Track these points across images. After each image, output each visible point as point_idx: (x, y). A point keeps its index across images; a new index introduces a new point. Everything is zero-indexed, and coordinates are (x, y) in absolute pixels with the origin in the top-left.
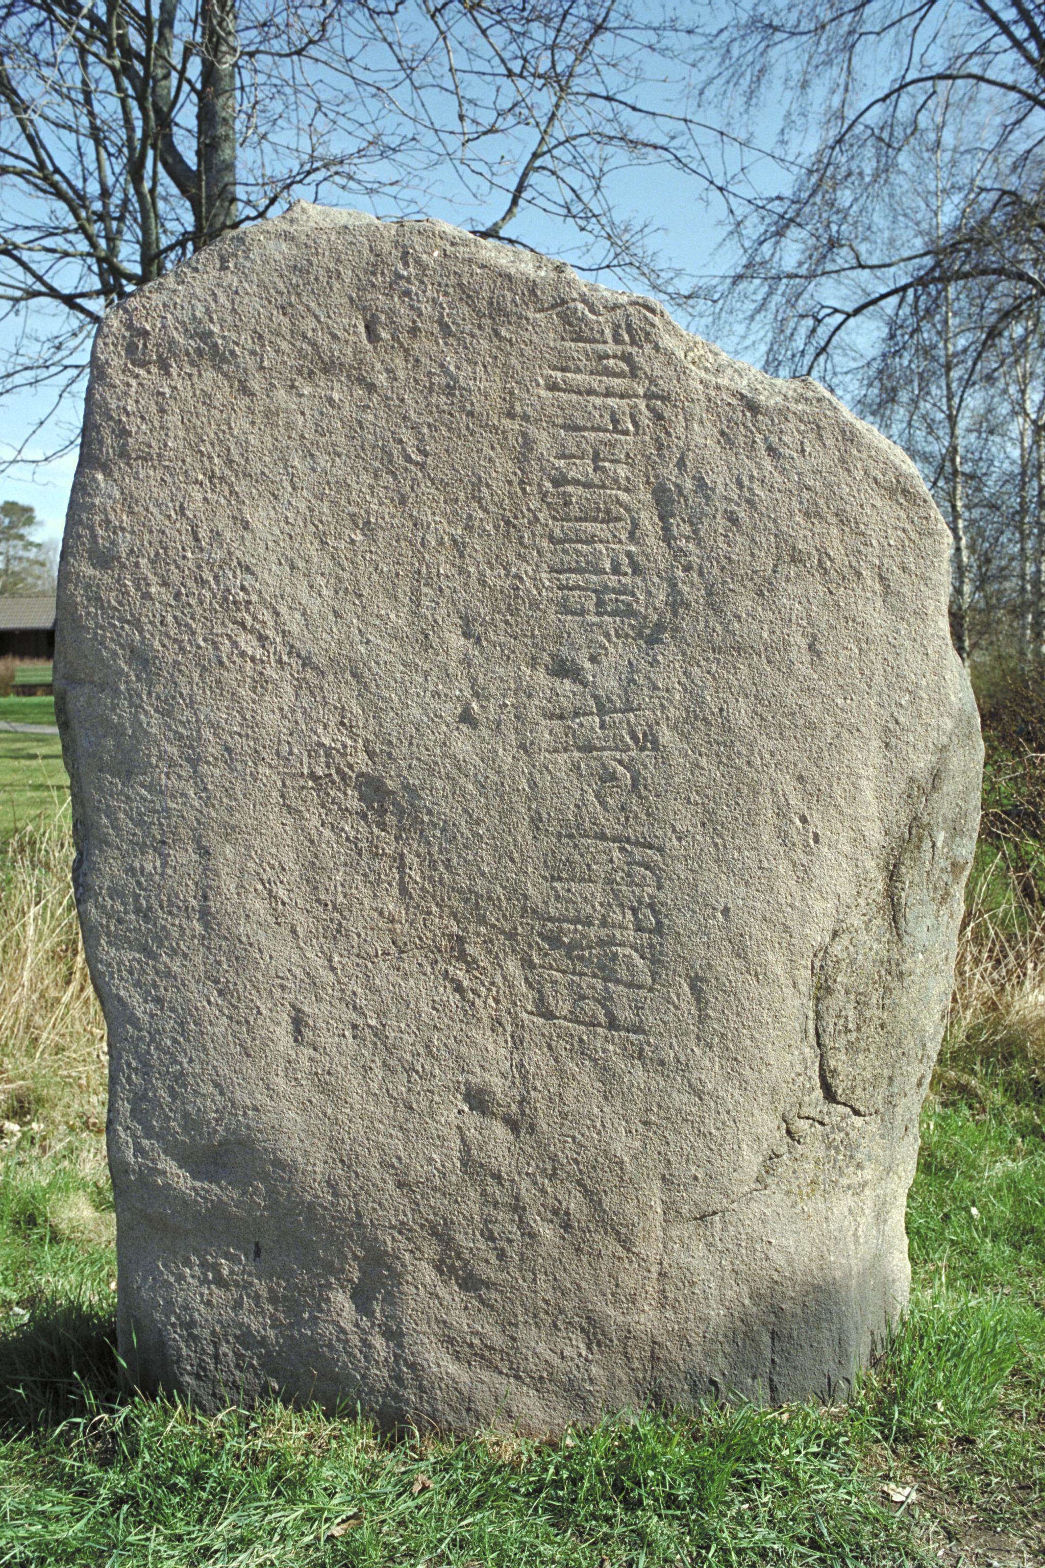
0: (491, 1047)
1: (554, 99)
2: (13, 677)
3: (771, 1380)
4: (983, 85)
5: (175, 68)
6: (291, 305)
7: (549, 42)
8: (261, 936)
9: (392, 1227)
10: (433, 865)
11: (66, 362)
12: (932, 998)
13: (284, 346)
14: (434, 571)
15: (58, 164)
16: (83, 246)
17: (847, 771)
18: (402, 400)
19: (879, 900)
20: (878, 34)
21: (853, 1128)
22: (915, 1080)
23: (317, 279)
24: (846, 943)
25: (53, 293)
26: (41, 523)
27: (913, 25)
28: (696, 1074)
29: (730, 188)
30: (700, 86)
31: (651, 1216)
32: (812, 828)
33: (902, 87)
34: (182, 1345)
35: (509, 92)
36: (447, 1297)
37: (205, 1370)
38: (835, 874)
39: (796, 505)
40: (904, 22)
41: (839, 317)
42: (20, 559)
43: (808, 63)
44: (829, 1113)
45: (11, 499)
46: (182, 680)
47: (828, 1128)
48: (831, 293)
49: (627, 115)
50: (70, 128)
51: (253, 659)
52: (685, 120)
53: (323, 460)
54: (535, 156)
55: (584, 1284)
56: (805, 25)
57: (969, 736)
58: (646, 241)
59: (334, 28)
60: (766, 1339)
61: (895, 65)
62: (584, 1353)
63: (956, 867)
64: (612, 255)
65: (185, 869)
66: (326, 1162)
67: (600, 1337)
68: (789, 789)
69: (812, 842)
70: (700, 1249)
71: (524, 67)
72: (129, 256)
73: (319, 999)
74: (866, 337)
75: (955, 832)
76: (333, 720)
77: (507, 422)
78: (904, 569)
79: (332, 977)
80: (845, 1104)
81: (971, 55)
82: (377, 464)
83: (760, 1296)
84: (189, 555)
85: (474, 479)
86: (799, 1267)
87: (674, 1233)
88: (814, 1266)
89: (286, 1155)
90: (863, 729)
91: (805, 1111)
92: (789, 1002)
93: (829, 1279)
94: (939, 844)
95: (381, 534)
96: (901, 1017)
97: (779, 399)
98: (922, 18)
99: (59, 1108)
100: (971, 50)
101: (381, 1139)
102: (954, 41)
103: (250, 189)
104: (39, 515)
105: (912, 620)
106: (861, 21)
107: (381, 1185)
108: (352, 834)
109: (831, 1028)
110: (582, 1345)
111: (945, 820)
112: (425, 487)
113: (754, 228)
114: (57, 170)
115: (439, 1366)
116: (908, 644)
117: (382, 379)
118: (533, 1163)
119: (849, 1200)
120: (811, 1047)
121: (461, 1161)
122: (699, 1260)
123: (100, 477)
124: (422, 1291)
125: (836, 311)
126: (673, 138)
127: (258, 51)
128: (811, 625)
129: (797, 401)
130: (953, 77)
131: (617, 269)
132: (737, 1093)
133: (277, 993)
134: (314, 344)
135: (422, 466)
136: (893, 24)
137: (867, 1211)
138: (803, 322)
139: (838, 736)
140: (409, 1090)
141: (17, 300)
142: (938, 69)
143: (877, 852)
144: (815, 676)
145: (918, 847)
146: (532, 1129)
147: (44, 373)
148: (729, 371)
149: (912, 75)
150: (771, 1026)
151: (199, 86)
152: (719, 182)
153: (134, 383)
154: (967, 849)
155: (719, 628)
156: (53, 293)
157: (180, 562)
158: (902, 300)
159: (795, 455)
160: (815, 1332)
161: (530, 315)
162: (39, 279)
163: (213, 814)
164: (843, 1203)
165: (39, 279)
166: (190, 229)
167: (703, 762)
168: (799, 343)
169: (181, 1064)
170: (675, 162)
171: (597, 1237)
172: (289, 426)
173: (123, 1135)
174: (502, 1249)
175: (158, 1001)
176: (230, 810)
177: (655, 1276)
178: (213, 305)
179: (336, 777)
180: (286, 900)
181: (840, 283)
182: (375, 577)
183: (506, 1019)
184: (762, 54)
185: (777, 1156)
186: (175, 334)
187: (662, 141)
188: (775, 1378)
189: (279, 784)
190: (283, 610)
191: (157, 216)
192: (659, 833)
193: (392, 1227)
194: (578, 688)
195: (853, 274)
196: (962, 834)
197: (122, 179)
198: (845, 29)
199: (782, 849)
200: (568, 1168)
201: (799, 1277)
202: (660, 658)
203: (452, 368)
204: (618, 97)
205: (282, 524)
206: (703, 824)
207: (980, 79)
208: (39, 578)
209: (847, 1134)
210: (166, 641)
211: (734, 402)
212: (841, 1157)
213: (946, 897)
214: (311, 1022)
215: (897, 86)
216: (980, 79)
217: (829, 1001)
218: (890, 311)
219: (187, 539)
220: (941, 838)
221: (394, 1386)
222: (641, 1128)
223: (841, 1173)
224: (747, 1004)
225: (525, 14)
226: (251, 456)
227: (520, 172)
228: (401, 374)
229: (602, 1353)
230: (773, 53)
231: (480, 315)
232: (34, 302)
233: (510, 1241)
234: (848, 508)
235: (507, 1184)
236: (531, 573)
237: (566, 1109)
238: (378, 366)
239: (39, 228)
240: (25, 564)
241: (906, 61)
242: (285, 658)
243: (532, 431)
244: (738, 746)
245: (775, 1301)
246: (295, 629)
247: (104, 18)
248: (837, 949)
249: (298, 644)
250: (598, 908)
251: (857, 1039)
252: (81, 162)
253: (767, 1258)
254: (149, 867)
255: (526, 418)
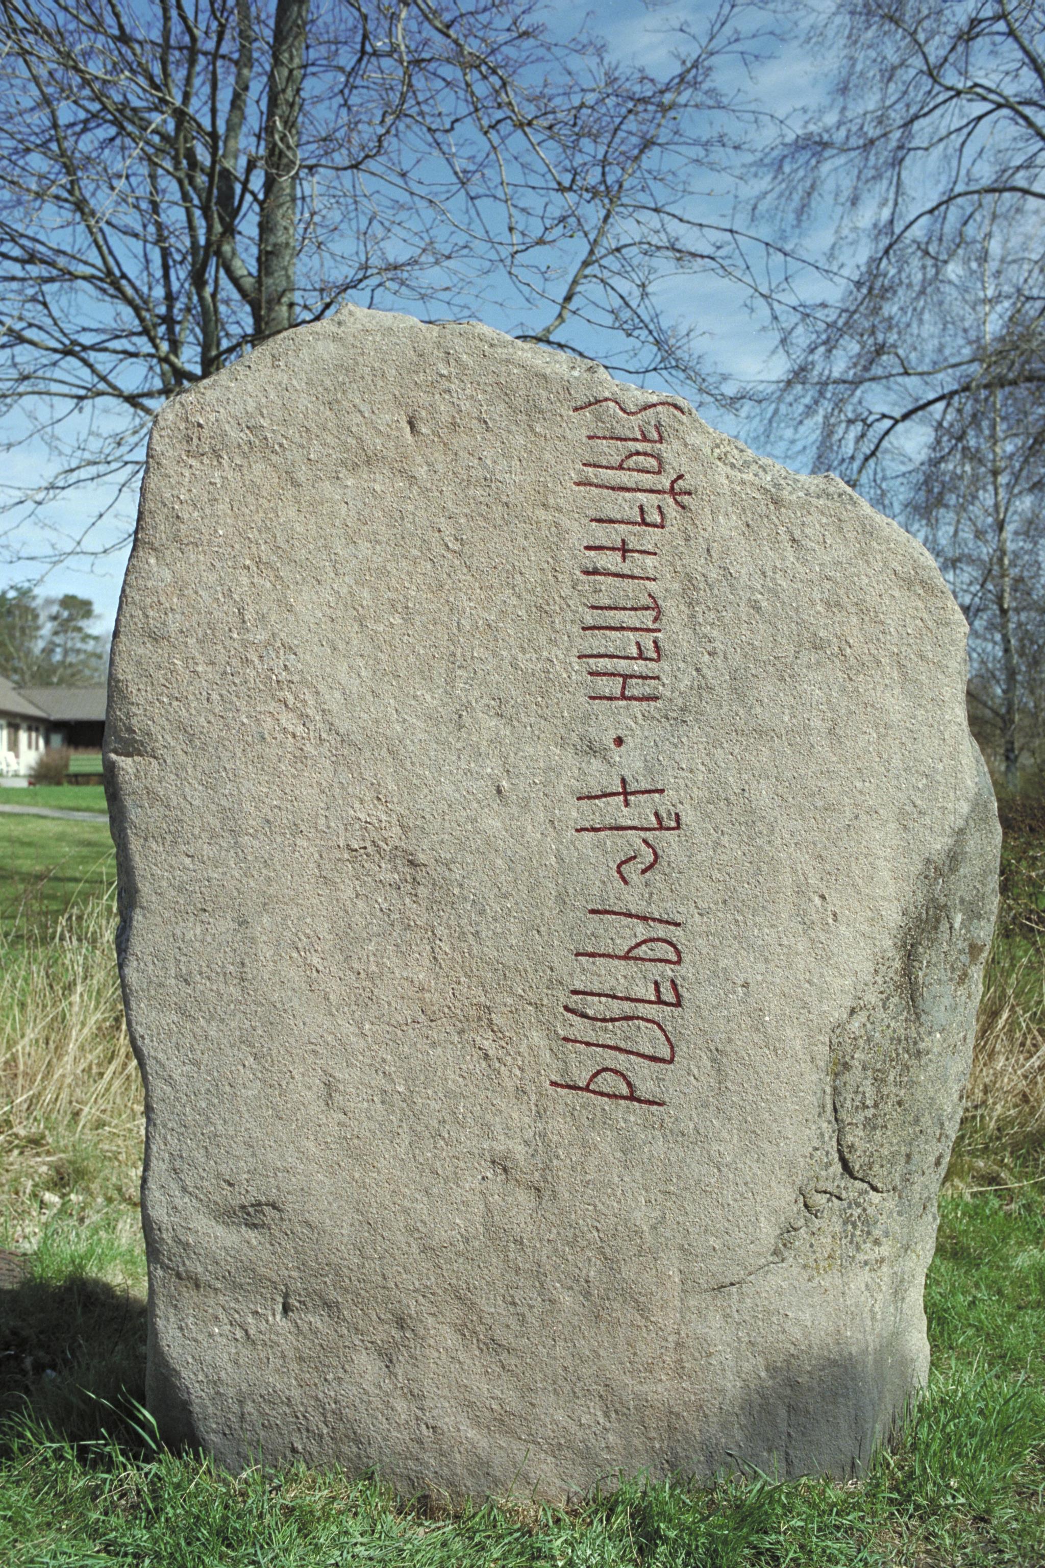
0: (515, 1115)
1: (603, 213)
2: (66, 766)
3: (787, 1454)
4: (1030, 199)
5: (236, 178)
6: (337, 401)
7: (600, 156)
8: (295, 1003)
9: (416, 1291)
10: (462, 936)
11: (127, 458)
12: (949, 1075)
13: (330, 439)
14: (468, 655)
15: (125, 269)
16: (148, 348)
17: (865, 851)
18: (441, 492)
19: (896, 978)
20: (926, 149)
21: (871, 1204)
22: (932, 1159)
23: (362, 378)
24: (864, 1020)
25: (118, 394)
26: (99, 617)
27: (961, 140)
28: (715, 1147)
29: (774, 296)
30: (752, 202)
31: (669, 1285)
32: (830, 908)
33: (950, 199)
34: (208, 1403)
35: (560, 203)
36: (468, 1361)
37: (230, 1428)
38: (852, 953)
39: (817, 596)
40: (953, 136)
41: (888, 423)
42: (78, 651)
43: (858, 178)
44: (846, 1188)
45: (71, 591)
46: (225, 755)
47: (845, 1203)
48: (878, 400)
49: (673, 226)
50: (136, 236)
51: (294, 736)
52: (731, 231)
53: (365, 548)
54: (586, 264)
55: (602, 1352)
56: (854, 142)
57: (985, 820)
58: (692, 344)
59: (391, 143)
60: (783, 1412)
61: (944, 178)
62: (601, 1421)
63: (974, 950)
64: (659, 358)
65: (223, 937)
66: (352, 1225)
67: (617, 1405)
68: (808, 869)
69: (831, 921)
70: (716, 1320)
71: (573, 181)
72: (189, 358)
73: (349, 1065)
74: (914, 442)
75: (974, 914)
76: (369, 796)
77: (541, 513)
78: (922, 657)
79: (362, 1044)
80: (862, 1180)
81: (1018, 168)
82: (415, 552)
83: (775, 1369)
84: (235, 636)
85: (508, 567)
86: (815, 1341)
87: (692, 1303)
88: (830, 1340)
89: (314, 1217)
90: (881, 812)
91: (822, 1186)
92: (807, 1076)
93: (846, 1354)
94: (957, 926)
95: (417, 618)
96: (919, 1095)
97: (801, 494)
98: (969, 134)
99: (98, 1180)
100: (1018, 163)
101: (407, 1204)
102: (1000, 155)
103: (306, 294)
104: (97, 609)
105: (929, 707)
106: (910, 136)
107: (406, 1249)
108: (385, 906)
109: (848, 1104)
110: (599, 1413)
111: (962, 901)
112: (462, 574)
113: (802, 337)
114: (124, 276)
115: (459, 1430)
116: (925, 729)
117: (422, 472)
118: (554, 1231)
119: (865, 1276)
120: (829, 1122)
121: (485, 1226)
122: (714, 1328)
123: (152, 561)
124: (444, 1356)
125: (884, 416)
126: (719, 248)
127: (316, 166)
128: (833, 710)
129: (818, 497)
130: (1001, 191)
131: (664, 372)
132: (755, 1165)
133: (310, 1059)
134: (360, 440)
135: (459, 554)
136: (941, 140)
137: (884, 1288)
138: (852, 427)
139: (857, 817)
140: (435, 1156)
141: (81, 398)
142: (985, 182)
143: (895, 932)
144: (835, 759)
145: (936, 928)
146: (555, 1196)
147: (102, 468)
148: (754, 467)
149: (959, 188)
150: (789, 1100)
151: (261, 196)
152: (765, 291)
153: (187, 473)
154: (986, 931)
155: (741, 712)
156: (118, 394)
157: (228, 642)
158: (948, 405)
159: (817, 547)
160: (831, 1407)
161: (564, 412)
162: (103, 379)
163: (252, 884)
164: (860, 1279)
165: (103, 379)
166: (250, 331)
167: (725, 840)
168: (849, 448)
169: (214, 1125)
170: (721, 271)
171: (616, 1305)
172: (332, 515)
173: (157, 1194)
174: (523, 1315)
175: (196, 1063)
176: (269, 880)
177: (672, 1345)
178: (264, 400)
179: (370, 849)
180: (321, 968)
181: (889, 388)
182: (412, 659)
183: (530, 1088)
184: (812, 170)
185: (795, 1230)
186: (227, 427)
187: (709, 250)
188: (791, 1452)
189: (316, 855)
190: (322, 688)
191: (217, 320)
192: (682, 909)
193: (416, 1291)
194: (604, 767)
195: (900, 379)
196: (979, 917)
197: (187, 285)
198: (893, 144)
199: (800, 927)
200: (589, 1236)
201: (815, 1351)
202: (684, 740)
203: (489, 462)
204: (668, 209)
205: (325, 608)
206: (725, 902)
207: (1026, 192)
208: (96, 670)
209: (864, 1210)
210: (211, 718)
211: (758, 496)
212: (858, 1233)
213: (964, 978)
214: (341, 1087)
215: (945, 198)
216: (1026, 192)
217: (847, 1077)
218: (938, 416)
219: (234, 620)
220: (958, 918)
221: (415, 1448)
222: (660, 1197)
223: (858, 1249)
224: (766, 1079)
225: (576, 129)
226: (296, 543)
227: (570, 279)
228: (440, 467)
229: (619, 1421)
230: (826, 168)
231: (515, 411)
232: (99, 400)
233: (531, 1307)
234: (868, 598)
235: (528, 1250)
236: (561, 657)
237: (588, 1177)
238: (419, 459)
239: (103, 331)
240: (82, 656)
241: (954, 174)
242: (324, 736)
243: (565, 522)
244: (760, 826)
245: (791, 1375)
246: (335, 708)
247: (173, 134)
248: (855, 1025)
249: (336, 722)
250: (622, 981)
251: (874, 1115)
252: (147, 268)
253: (784, 1332)
254: (190, 935)
255: (559, 509)
